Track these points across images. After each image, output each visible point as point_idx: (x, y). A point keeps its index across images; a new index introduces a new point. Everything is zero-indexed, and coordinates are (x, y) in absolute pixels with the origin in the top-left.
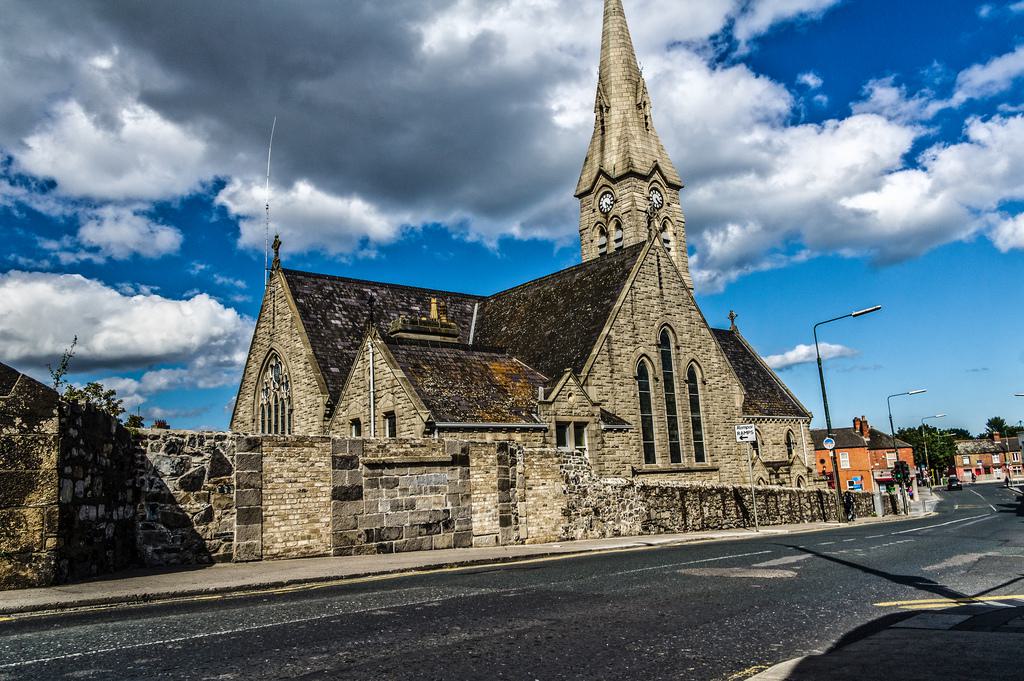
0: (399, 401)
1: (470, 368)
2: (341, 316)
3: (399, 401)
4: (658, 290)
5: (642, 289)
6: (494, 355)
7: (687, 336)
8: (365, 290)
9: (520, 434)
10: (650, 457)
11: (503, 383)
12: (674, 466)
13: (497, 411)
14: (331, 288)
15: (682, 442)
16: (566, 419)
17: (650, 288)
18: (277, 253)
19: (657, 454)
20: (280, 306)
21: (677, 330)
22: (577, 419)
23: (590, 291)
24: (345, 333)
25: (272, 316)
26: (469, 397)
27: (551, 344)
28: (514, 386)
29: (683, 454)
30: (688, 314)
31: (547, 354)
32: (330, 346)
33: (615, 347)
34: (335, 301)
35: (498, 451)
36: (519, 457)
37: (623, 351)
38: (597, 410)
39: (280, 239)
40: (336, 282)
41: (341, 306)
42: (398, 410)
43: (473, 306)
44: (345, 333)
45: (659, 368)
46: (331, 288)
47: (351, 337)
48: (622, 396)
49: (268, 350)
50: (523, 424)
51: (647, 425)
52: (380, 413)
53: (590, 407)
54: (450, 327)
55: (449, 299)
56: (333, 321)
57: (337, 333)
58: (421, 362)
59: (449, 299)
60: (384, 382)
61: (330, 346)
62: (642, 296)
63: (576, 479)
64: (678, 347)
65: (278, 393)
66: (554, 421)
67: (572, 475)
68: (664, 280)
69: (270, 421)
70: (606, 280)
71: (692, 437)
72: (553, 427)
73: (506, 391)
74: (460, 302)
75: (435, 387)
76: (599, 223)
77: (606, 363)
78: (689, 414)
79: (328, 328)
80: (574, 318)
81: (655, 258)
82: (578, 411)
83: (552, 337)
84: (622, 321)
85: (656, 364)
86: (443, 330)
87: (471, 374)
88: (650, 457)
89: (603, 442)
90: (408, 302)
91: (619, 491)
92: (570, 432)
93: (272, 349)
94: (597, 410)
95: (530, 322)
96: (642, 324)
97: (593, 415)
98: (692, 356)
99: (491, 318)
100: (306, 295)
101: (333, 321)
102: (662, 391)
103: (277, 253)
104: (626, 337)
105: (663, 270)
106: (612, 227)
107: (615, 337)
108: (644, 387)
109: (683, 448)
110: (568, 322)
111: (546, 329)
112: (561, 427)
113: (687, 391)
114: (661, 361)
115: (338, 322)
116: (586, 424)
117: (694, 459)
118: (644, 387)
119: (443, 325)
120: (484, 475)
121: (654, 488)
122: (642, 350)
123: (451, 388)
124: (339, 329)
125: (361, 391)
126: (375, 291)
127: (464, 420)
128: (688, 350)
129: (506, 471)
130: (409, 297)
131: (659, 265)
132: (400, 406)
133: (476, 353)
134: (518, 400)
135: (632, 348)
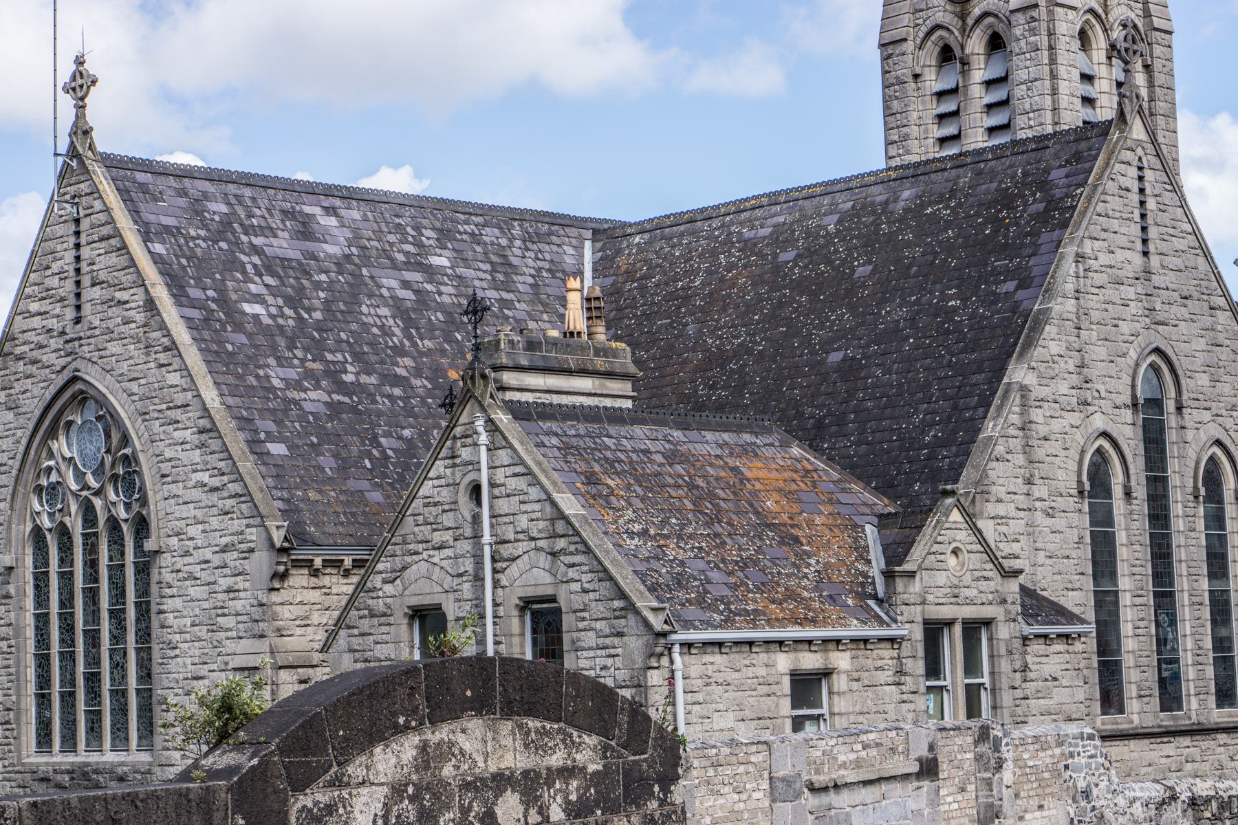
0: (572, 573)
1: (705, 477)
2: (263, 291)
3: (572, 573)
4: (1138, 259)
5: (1104, 259)
6: (747, 437)
7: (1203, 380)
8: (307, 209)
9: (848, 654)
10: (1111, 698)
11: (785, 517)
12: (1166, 720)
13: (791, 595)
14: (224, 209)
15: (1187, 658)
16: (946, 612)
17: (1120, 255)
18: (81, 107)
19: (1130, 691)
20: (102, 262)
21: (1181, 364)
22: (969, 612)
23: (950, 249)
24: (282, 342)
25: (69, 285)
26: (723, 561)
27: (851, 394)
28: (810, 523)
29: (1189, 687)
30: (1207, 321)
31: (841, 421)
32: (252, 380)
33: (1037, 415)
34: (238, 243)
35: (976, 743)
36: (1008, 754)
37: (1056, 425)
38: (1013, 586)
39: (90, 67)
40: (231, 188)
41: (256, 260)
42: (568, 598)
43: (579, 248)
44: (282, 342)
45: (1137, 466)
46: (224, 209)
47: (299, 353)
48: (1053, 543)
49: (60, 380)
50: (855, 629)
51: (1106, 604)
52: (512, 600)
53: (996, 583)
54: (615, 353)
55: (517, 231)
56: (248, 308)
57: (261, 340)
58: (597, 468)
59: (517, 231)
60: (523, 522)
61: (252, 380)
62: (1100, 279)
63: (1087, 794)
64: (1179, 409)
65: (98, 503)
66: (919, 619)
67: (1082, 785)
68: (1153, 232)
69: (66, 578)
70: (997, 222)
71: (1208, 643)
72: (918, 633)
73: (796, 540)
74: (540, 237)
75: (644, 533)
76: (937, 27)
77: (1020, 459)
78: (1205, 584)
79: (239, 328)
80: (912, 322)
81: (1133, 172)
82: (972, 593)
83: (850, 370)
84: (1054, 348)
85: (1129, 458)
86: (600, 363)
87: (711, 495)
88: (1111, 698)
89: (1025, 668)
90: (418, 244)
91: (1153, 812)
92: (952, 646)
93: (74, 379)
94: (1013, 586)
95: (772, 319)
96: (1100, 351)
97: (1004, 601)
98: (1215, 432)
99: (643, 289)
100: (167, 229)
101: (248, 308)
102: (1141, 526)
103: (81, 107)
104: (1063, 388)
105: (1151, 204)
106: (976, 45)
107: (1038, 392)
108: (1102, 519)
109: (1189, 673)
110: (895, 333)
111: (827, 347)
112: (934, 631)
113: (1201, 525)
114: (1141, 450)
115: (258, 309)
116: (988, 623)
117: (1212, 700)
118: (1102, 519)
119: (601, 351)
120: (960, 797)
121: (1208, 800)
122: (1099, 422)
123: (680, 537)
124: (267, 331)
125: (447, 536)
126: (331, 211)
127: (727, 623)
128: (1206, 416)
129: (989, 783)
130: (417, 228)
131: (1142, 191)
132: (576, 587)
133: (709, 436)
134: (827, 565)
135: (1075, 418)
